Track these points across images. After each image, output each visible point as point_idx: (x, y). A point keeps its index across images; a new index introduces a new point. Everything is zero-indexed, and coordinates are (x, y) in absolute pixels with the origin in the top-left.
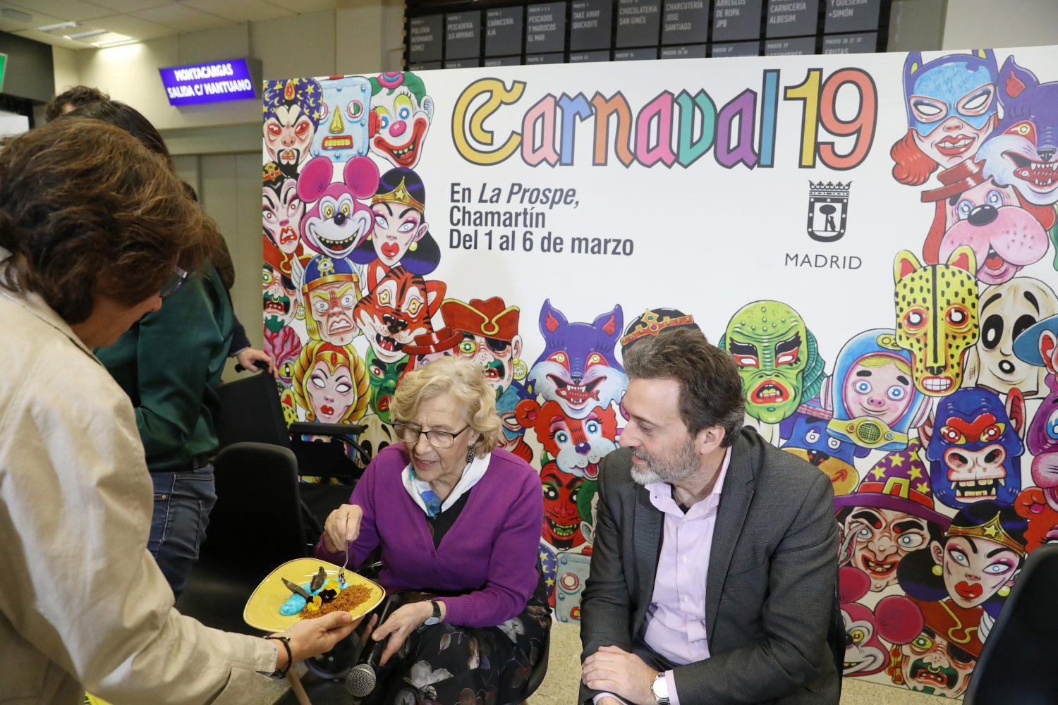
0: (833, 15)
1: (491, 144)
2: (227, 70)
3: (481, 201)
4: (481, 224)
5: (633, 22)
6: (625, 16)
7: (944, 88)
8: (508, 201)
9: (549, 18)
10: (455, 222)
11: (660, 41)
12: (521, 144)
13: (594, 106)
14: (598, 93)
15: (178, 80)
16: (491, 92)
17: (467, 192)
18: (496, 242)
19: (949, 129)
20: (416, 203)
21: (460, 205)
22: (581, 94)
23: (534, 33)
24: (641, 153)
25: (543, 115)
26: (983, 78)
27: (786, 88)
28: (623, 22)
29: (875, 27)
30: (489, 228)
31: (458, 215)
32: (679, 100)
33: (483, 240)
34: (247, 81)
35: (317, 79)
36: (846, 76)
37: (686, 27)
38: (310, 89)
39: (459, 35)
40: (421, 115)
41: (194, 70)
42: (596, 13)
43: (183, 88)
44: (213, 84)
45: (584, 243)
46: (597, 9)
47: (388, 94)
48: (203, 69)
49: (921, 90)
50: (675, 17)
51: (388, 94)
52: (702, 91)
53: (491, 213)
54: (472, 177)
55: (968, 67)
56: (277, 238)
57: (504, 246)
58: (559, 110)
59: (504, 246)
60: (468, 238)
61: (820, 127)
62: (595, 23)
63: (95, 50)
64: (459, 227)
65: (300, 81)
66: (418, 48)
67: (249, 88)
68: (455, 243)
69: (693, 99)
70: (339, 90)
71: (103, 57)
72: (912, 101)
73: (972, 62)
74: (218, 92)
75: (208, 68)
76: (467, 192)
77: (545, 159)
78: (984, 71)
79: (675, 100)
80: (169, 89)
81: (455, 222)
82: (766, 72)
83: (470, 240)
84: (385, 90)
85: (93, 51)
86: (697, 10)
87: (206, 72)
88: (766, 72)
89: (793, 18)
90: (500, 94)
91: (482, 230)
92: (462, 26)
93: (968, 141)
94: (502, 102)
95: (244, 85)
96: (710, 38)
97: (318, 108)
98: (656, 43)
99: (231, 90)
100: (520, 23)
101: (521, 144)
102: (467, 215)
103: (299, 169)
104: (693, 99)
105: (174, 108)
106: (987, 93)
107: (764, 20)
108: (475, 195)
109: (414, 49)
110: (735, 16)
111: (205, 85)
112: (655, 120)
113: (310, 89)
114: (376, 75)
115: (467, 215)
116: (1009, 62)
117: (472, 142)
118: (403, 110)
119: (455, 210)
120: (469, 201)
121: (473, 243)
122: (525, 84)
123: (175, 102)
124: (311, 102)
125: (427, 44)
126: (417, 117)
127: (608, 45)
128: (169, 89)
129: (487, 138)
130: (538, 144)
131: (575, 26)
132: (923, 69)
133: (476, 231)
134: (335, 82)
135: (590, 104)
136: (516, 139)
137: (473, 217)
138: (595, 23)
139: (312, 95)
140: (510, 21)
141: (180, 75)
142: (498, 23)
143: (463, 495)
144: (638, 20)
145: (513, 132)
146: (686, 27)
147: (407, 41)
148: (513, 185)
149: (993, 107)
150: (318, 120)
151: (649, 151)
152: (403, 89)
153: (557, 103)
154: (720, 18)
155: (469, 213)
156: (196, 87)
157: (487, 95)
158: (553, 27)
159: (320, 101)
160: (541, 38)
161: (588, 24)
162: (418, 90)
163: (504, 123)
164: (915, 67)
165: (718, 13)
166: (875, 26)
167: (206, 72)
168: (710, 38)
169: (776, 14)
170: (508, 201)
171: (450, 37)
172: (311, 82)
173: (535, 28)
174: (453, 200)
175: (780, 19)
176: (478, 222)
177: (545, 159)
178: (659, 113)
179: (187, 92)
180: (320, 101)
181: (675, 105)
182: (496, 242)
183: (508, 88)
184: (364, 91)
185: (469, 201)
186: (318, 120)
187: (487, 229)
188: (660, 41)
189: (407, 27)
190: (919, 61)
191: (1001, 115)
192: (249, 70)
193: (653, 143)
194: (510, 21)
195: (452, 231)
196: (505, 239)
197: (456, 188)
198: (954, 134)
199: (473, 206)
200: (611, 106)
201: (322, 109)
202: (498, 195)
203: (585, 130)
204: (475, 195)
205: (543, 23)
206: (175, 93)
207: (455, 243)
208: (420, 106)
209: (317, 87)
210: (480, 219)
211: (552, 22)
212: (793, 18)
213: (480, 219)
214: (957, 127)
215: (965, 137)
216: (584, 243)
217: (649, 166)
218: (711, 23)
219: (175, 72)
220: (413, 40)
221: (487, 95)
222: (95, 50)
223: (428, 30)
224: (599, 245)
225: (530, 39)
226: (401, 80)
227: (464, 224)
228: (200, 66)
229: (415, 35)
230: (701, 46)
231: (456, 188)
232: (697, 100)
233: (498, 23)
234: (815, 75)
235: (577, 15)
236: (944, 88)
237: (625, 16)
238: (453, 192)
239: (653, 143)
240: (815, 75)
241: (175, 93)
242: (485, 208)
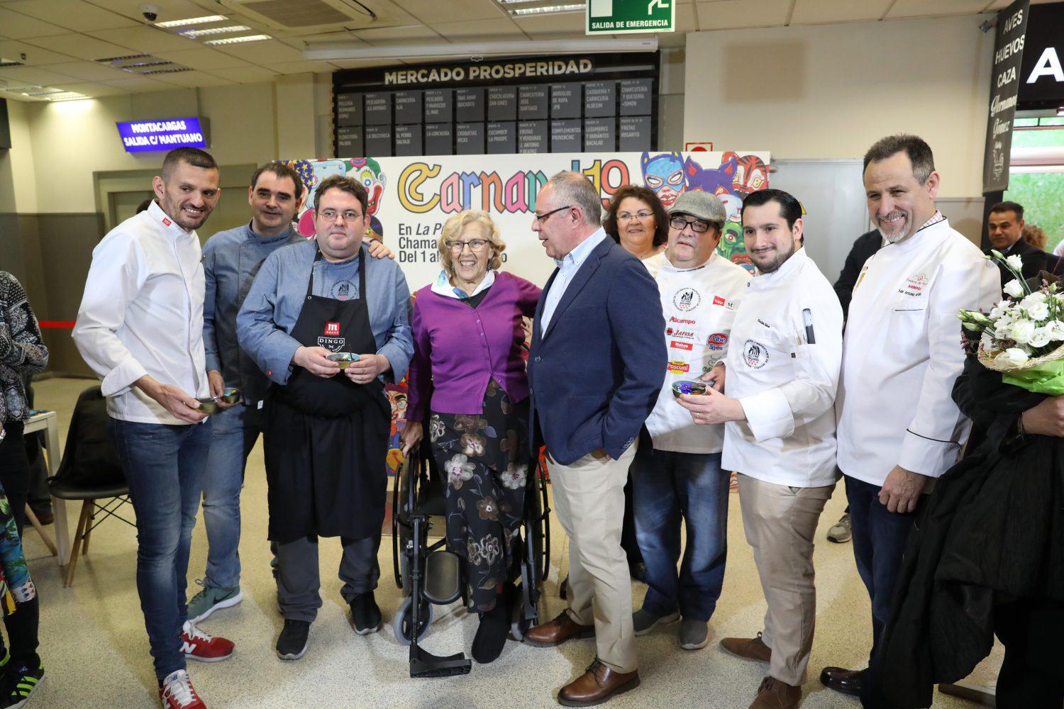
0: (625, 104)
1: (422, 201)
2: (181, 125)
3: (417, 234)
4: (418, 247)
5: (499, 104)
6: (493, 100)
7: (660, 170)
8: (434, 233)
9: (440, 99)
10: (402, 246)
11: (517, 117)
12: (440, 200)
13: (482, 179)
14: (483, 172)
15: (134, 132)
16: (421, 170)
17: (409, 229)
18: (428, 257)
19: (665, 191)
20: (377, 236)
21: (405, 236)
22: (473, 172)
23: (430, 109)
24: (509, 205)
25: (452, 184)
26: (677, 167)
27: (584, 170)
28: (492, 103)
29: (650, 113)
30: (423, 249)
31: (404, 242)
32: (528, 176)
33: (420, 257)
34: (199, 135)
35: (309, 161)
36: (614, 164)
37: (534, 108)
38: (305, 167)
39: (375, 108)
40: (379, 183)
41: (150, 125)
42: (474, 97)
43: (139, 139)
44: (167, 136)
45: (427, 243)
46: (474, 94)
47: (357, 171)
48: (159, 124)
49: (650, 172)
50: (526, 102)
51: (357, 171)
52: (540, 171)
53: (425, 241)
54: (412, 220)
55: (671, 161)
56: (397, 259)
57: (433, 260)
58: (461, 182)
59: (433, 260)
60: (410, 256)
61: (602, 190)
62: (473, 104)
63: (48, 102)
64: (405, 249)
65: (298, 161)
66: (345, 116)
67: (200, 140)
68: (403, 259)
69: (535, 176)
70: (325, 168)
71: (54, 109)
72: (646, 177)
73: (673, 159)
74: (172, 142)
75: (163, 124)
76: (409, 229)
77: (454, 209)
78: (678, 162)
79: (525, 176)
80: (125, 139)
81: (402, 246)
82: (573, 161)
83: (412, 257)
84: (354, 169)
85: (45, 104)
86: (540, 98)
87: (161, 127)
88: (573, 161)
89: (601, 105)
90: (426, 172)
91: (419, 251)
92: (377, 102)
93: (674, 197)
94: (427, 177)
95: (196, 138)
96: (549, 116)
97: (310, 178)
98: (515, 118)
99: (184, 141)
100: (420, 101)
101: (440, 200)
102: (409, 243)
103: (299, 216)
104: (535, 176)
105: (128, 153)
106: (680, 173)
107: (583, 105)
108: (414, 231)
109: (341, 116)
110: (564, 103)
111: (160, 137)
112: (515, 187)
113: (305, 167)
114: (349, 159)
115: (409, 243)
116: (689, 159)
117: (411, 200)
118: (366, 181)
119: (402, 239)
120: (410, 234)
121: (414, 258)
122: (440, 166)
123: (130, 149)
124: (306, 175)
125: (350, 113)
126: (376, 185)
127: (483, 119)
128: (125, 139)
129: (419, 197)
130: (450, 201)
131: (460, 105)
132: (650, 161)
133: (415, 252)
134: (322, 163)
135: (479, 178)
136: (437, 198)
137: (413, 244)
138: (473, 104)
139: (306, 171)
140: (412, 100)
141: (136, 128)
142: (404, 100)
143: (483, 291)
144: (502, 103)
145: (435, 194)
146: (534, 108)
147: (335, 110)
148: (436, 224)
149: (683, 181)
150: (311, 186)
151: (513, 204)
152: (367, 168)
153: (460, 178)
154: (555, 104)
155: (411, 241)
156: (152, 138)
157: (418, 173)
158: (444, 105)
159: (312, 174)
160: (436, 112)
161: (468, 104)
162: (376, 169)
163: (430, 188)
164: (646, 160)
165: (554, 100)
166: (649, 112)
167: (161, 127)
168: (549, 116)
169: (590, 96)
170: (434, 233)
171: (369, 109)
172: (305, 163)
173: (431, 106)
174: (400, 234)
175: (593, 106)
176: (416, 246)
177: (454, 209)
178: (517, 183)
179: (143, 141)
180: (312, 174)
181: (526, 179)
182: (428, 257)
183: (431, 169)
184: (341, 169)
185: (410, 234)
186: (311, 186)
187: (422, 250)
188: (517, 117)
189: (335, 100)
190: (648, 157)
191: (687, 184)
192: (201, 127)
193: (515, 200)
194: (412, 100)
195: (401, 252)
196: (433, 256)
197: (402, 227)
198: (667, 194)
199: (413, 237)
200: (491, 179)
201: (314, 180)
202: (428, 230)
203: (476, 193)
204: (414, 231)
205: (436, 102)
206: (130, 142)
207: (403, 259)
208: (377, 177)
209: (309, 166)
210: (418, 244)
211: (443, 102)
212: (601, 105)
213: (418, 244)
214: (668, 190)
215: (672, 195)
216: (427, 243)
217: (513, 212)
218: (550, 107)
219: (132, 126)
220: (340, 110)
221: (418, 173)
222: (48, 102)
223: (351, 104)
224: (418, 243)
225: (427, 112)
226: (364, 163)
227: (408, 247)
228: (156, 123)
229: (341, 107)
230: (543, 122)
231: (402, 227)
232: (538, 176)
233: (404, 100)
234: (598, 163)
235: (460, 98)
236: (660, 170)
237: (493, 100)
238: (400, 229)
239: (515, 200)
240: (598, 163)
241: (130, 142)
242: (420, 238)
